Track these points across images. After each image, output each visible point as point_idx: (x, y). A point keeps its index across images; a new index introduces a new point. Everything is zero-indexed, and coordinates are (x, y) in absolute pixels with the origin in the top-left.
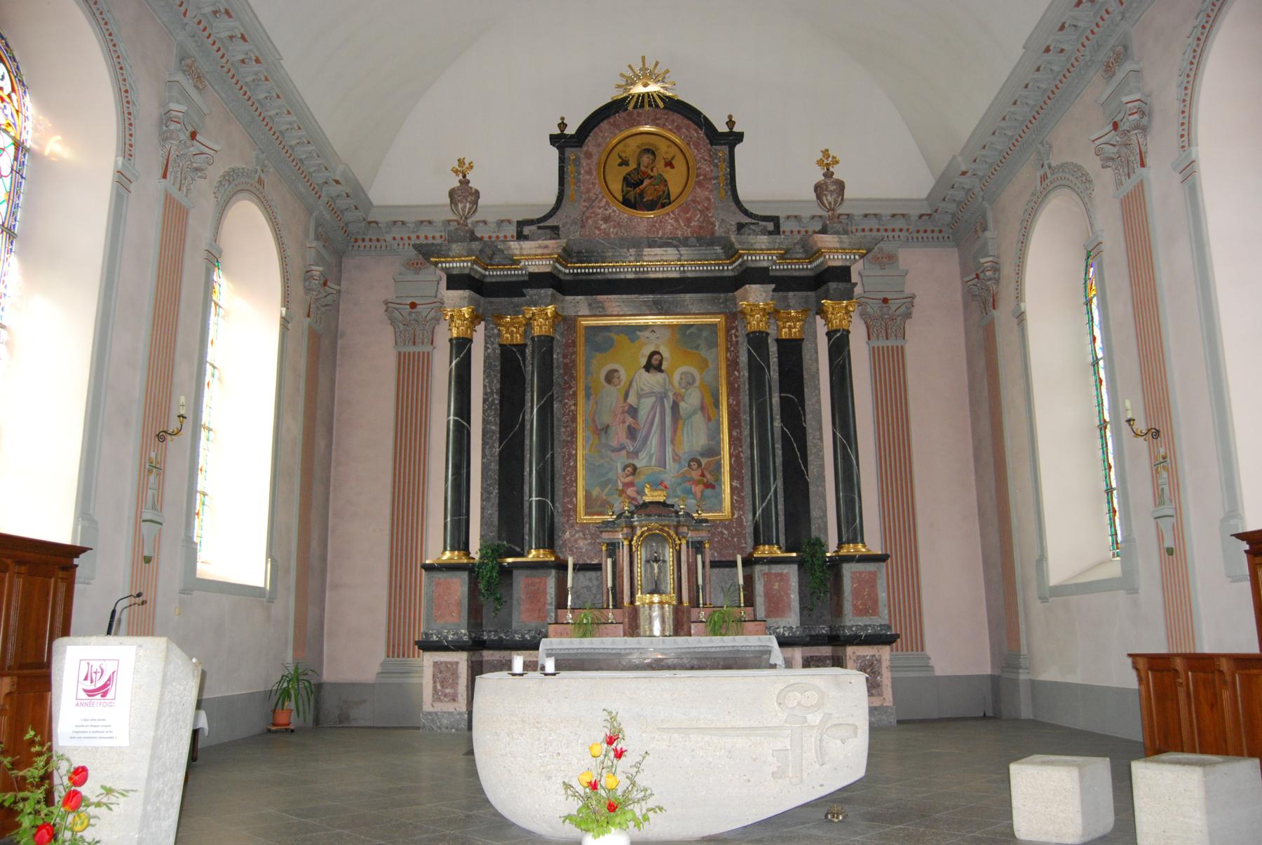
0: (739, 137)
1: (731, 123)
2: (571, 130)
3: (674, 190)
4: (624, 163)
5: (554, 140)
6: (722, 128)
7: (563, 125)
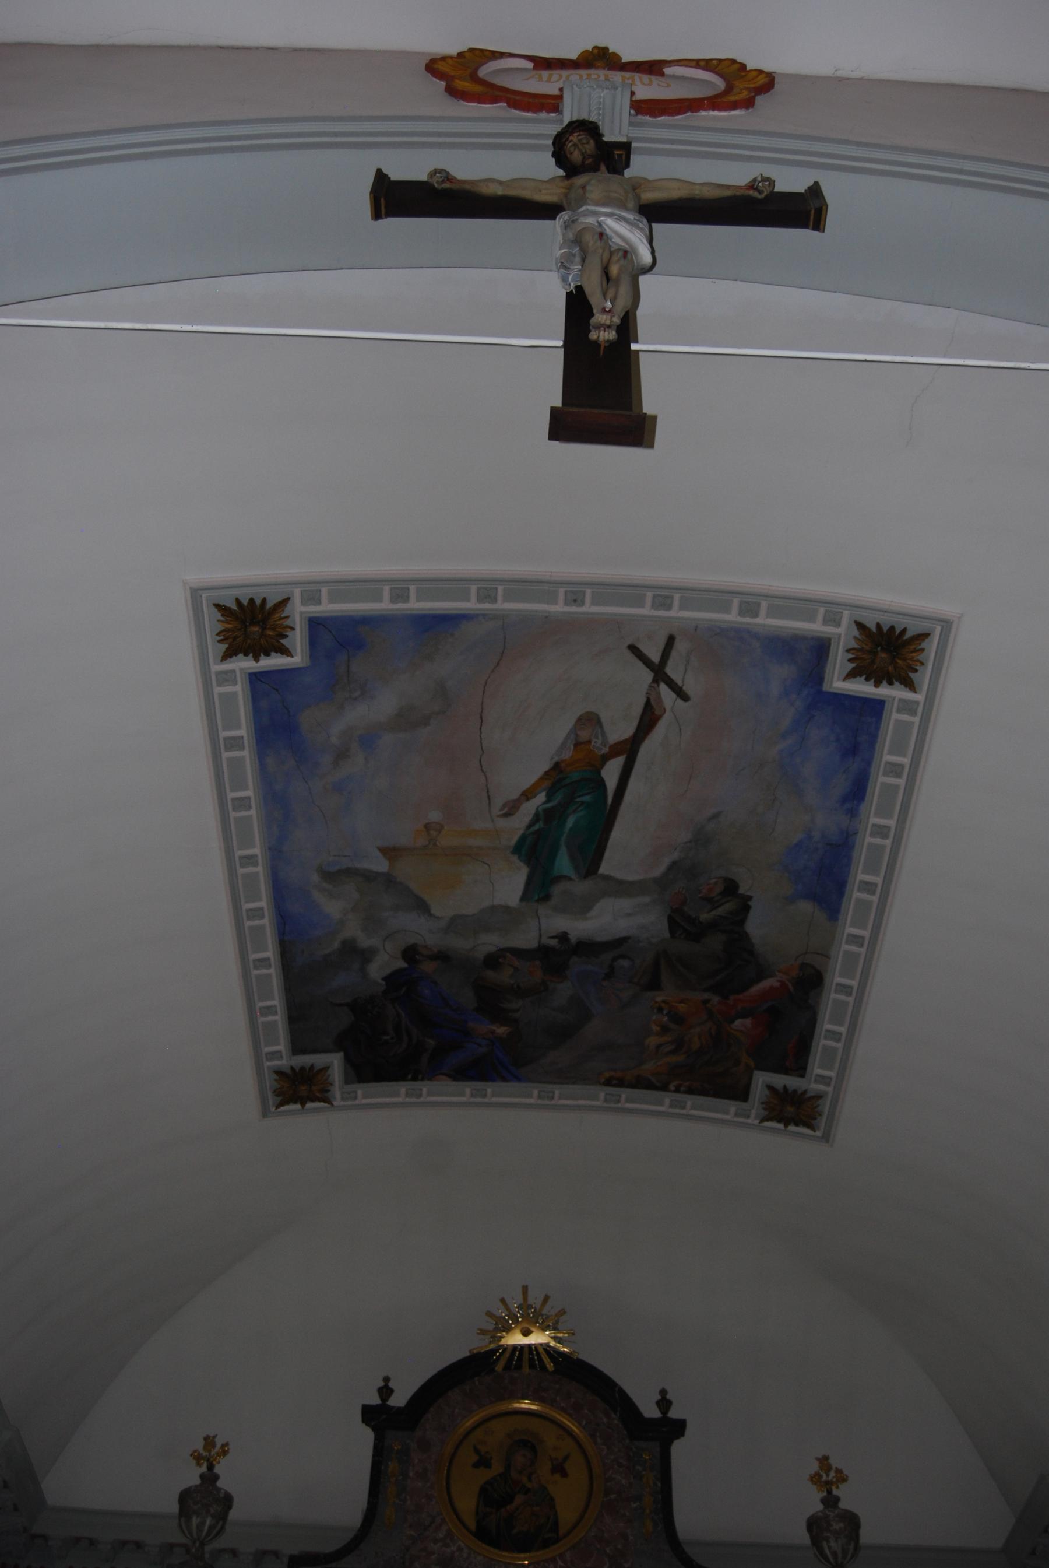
0: (678, 1428)
1: (664, 1403)
2: (399, 1400)
3: (566, 1515)
4: (483, 1462)
5: (369, 1414)
6: (650, 1411)
7: (385, 1391)
